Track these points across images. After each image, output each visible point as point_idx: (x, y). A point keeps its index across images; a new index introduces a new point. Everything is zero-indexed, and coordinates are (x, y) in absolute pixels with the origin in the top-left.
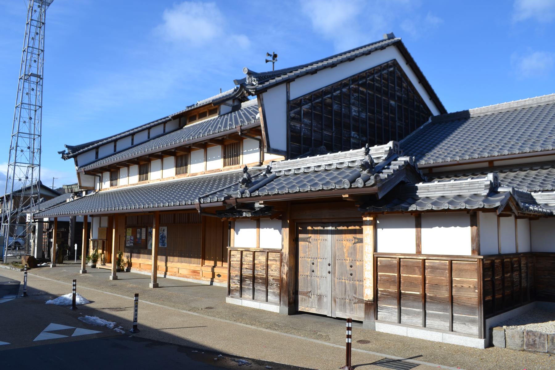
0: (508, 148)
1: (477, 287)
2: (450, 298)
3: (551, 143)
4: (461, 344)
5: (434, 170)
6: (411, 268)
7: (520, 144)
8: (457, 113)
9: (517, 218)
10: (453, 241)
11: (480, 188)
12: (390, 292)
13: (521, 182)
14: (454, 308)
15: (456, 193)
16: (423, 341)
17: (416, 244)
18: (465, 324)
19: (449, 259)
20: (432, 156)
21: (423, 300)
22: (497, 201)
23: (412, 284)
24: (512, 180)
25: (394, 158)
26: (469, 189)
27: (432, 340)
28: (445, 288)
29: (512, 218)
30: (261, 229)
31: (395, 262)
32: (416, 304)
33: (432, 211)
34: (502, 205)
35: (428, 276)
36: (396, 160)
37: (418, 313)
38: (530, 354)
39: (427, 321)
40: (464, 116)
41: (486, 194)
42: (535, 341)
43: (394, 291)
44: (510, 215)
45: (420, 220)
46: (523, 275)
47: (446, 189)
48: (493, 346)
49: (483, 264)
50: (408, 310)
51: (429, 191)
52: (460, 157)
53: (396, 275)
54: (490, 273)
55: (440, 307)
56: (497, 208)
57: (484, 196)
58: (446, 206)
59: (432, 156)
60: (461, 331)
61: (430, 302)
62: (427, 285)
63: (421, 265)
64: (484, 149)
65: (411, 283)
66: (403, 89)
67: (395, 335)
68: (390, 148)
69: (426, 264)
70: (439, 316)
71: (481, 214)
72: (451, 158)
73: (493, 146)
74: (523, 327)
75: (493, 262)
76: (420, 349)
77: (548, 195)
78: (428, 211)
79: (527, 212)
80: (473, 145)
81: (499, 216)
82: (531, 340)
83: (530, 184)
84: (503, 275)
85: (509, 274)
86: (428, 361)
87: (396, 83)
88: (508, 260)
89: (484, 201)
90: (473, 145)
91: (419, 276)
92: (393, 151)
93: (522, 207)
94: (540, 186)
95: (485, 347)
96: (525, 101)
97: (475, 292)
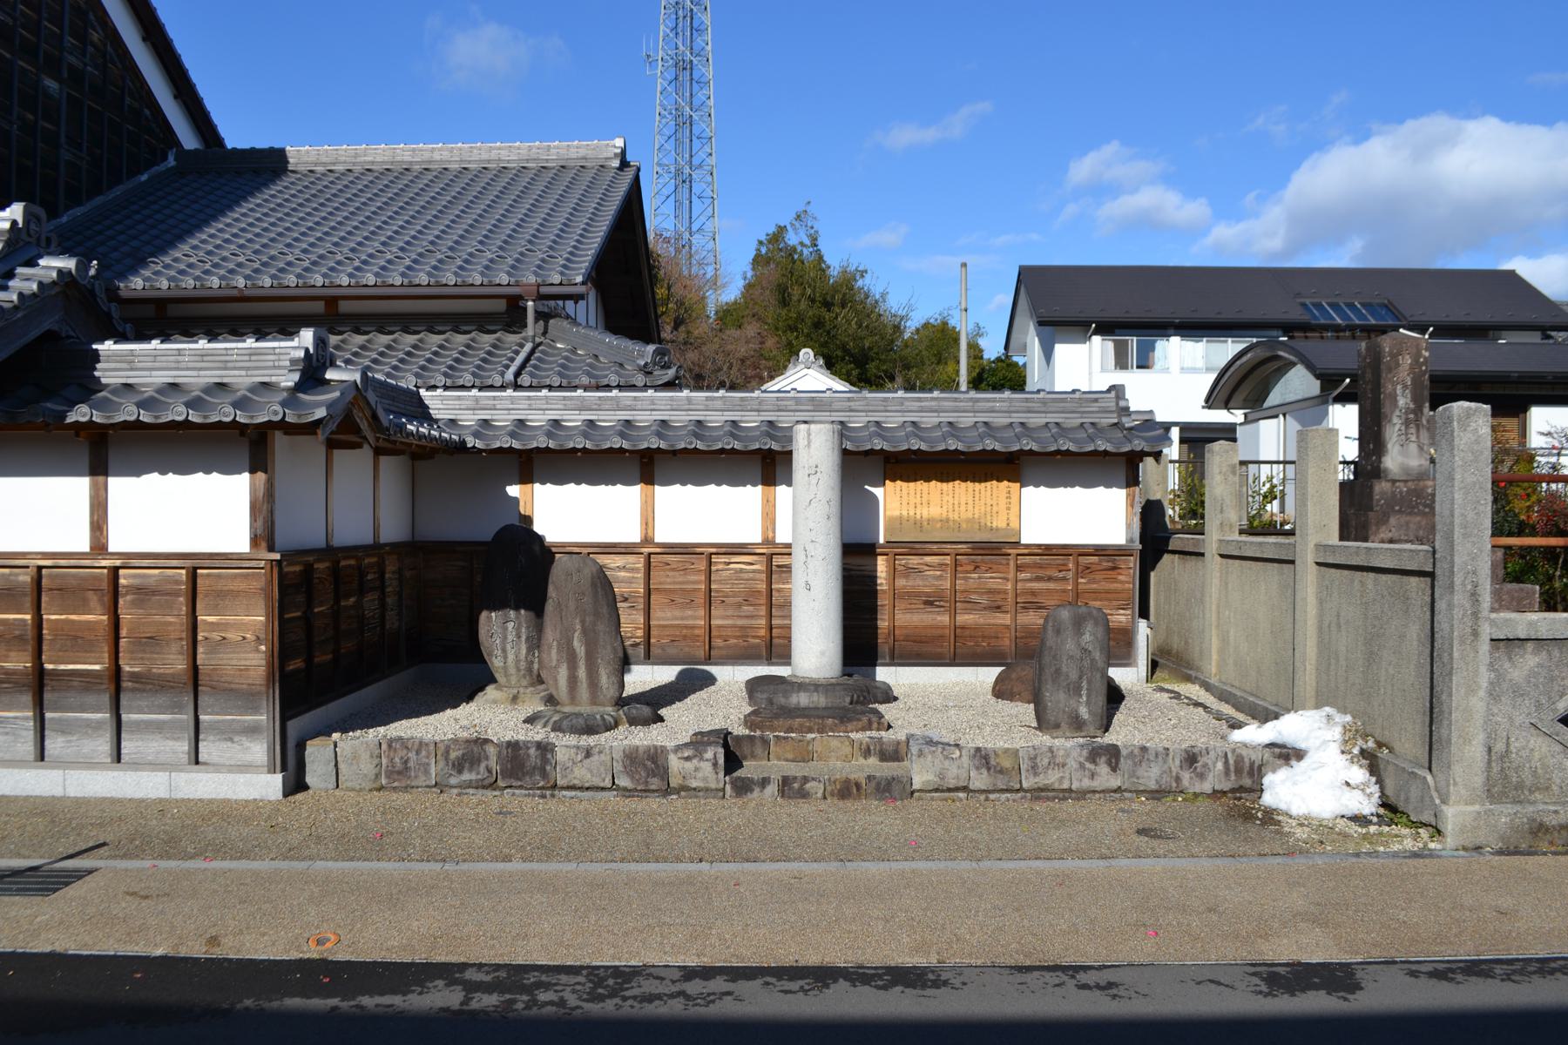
0: (376, 269)
1: (262, 636)
2: (191, 673)
3: (480, 268)
4: (221, 796)
5: (173, 310)
6: (72, 594)
7: (407, 262)
8: (253, 151)
9: (378, 452)
10: (195, 514)
11: (279, 367)
12: (8, 672)
13: (402, 361)
14: (203, 700)
15: (211, 377)
16: (113, 801)
17: (92, 523)
18: (231, 740)
19: (188, 563)
20: (167, 267)
21: (113, 687)
22: (318, 405)
23: (76, 640)
24: (382, 354)
25: (27, 257)
26: (248, 369)
27: (139, 795)
28: (175, 647)
29: (366, 454)
30: (659, 490)
31: (25, 578)
32: (91, 699)
33: (138, 425)
34: (330, 416)
35: (126, 617)
36: (32, 263)
37: (97, 726)
38: (394, 796)
39: (123, 744)
40: (269, 164)
41: (291, 384)
42: (406, 762)
43: (20, 666)
44: (358, 446)
45: (104, 451)
46: (389, 601)
47: (183, 365)
48: (305, 787)
49: (282, 576)
50: (66, 720)
51: (131, 365)
52: (247, 277)
53: (28, 617)
54: (301, 598)
55: (161, 700)
56: (319, 422)
57: (287, 389)
58: (178, 413)
59: (167, 267)
60: (222, 761)
61: (133, 690)
62: (123, 642)
63: (105, 585)
64: (314, 263)
65: (76, 638)
66: (91, 49)
67: (27, 798)
68: (14, 223)
69: (122, 581)
70: (158, 727)
71: (279, 439)
72: (222, 278)
73: (339, 257)
74: (382, 730)
75: (308, 570)
76: (101, 825)
77: (459, 398)
78: (125, 425)
79: (399, 437)
80: (286, 250)
81: (332, 445)
82: (397, 760)
83: (423, 368)
84: (337, 600)
85: (352, 600)
86: (124, 856)
87: (67, 22)
88: (352, 562)
89: (284, 404)
90: (286, 250)
91: (99, 618)
92: (24, 237)
93: (385, 423)
94: (446, 375)
95: (285, 795)
96: (433, 150)
97: (258, 651)
